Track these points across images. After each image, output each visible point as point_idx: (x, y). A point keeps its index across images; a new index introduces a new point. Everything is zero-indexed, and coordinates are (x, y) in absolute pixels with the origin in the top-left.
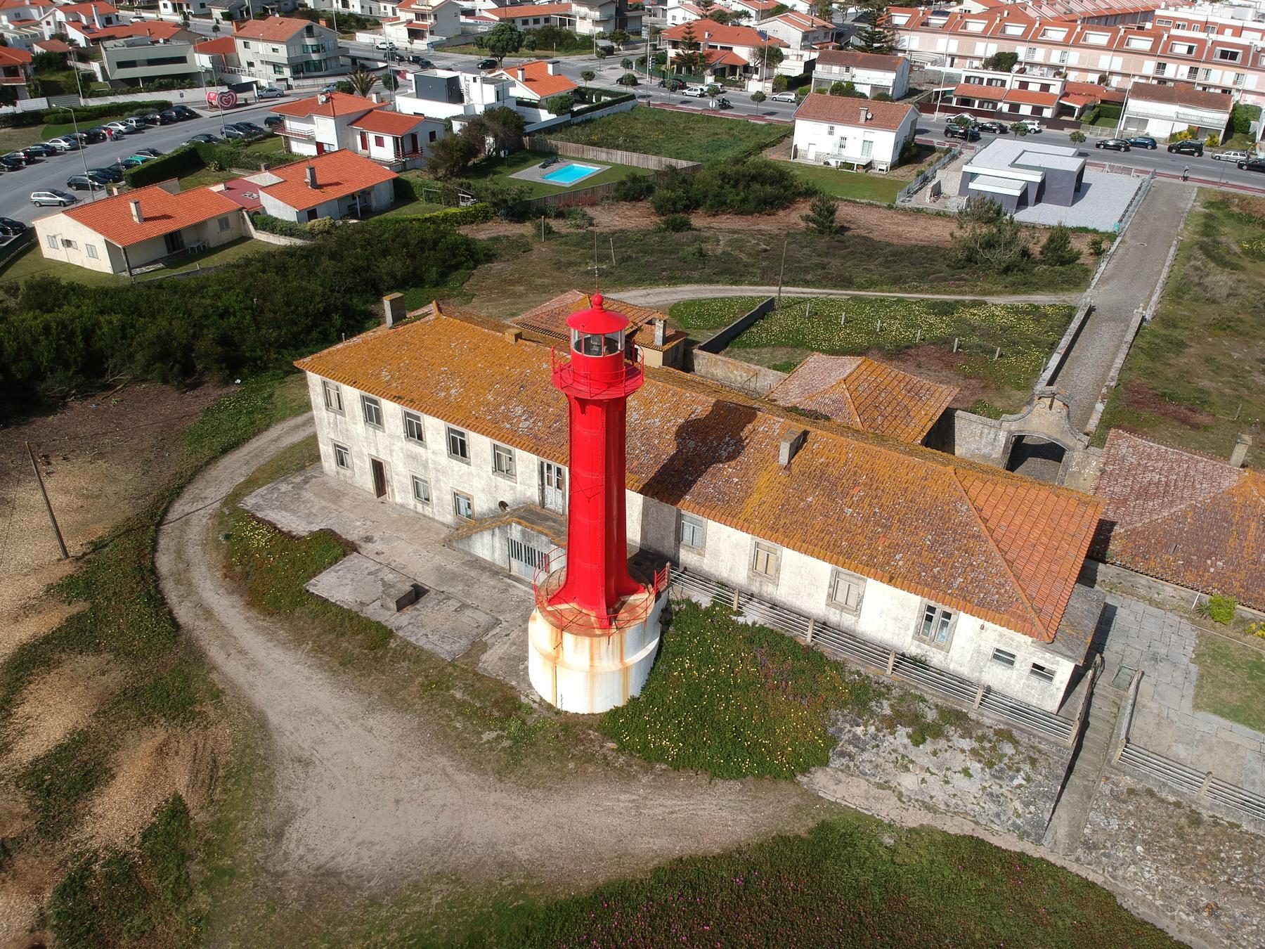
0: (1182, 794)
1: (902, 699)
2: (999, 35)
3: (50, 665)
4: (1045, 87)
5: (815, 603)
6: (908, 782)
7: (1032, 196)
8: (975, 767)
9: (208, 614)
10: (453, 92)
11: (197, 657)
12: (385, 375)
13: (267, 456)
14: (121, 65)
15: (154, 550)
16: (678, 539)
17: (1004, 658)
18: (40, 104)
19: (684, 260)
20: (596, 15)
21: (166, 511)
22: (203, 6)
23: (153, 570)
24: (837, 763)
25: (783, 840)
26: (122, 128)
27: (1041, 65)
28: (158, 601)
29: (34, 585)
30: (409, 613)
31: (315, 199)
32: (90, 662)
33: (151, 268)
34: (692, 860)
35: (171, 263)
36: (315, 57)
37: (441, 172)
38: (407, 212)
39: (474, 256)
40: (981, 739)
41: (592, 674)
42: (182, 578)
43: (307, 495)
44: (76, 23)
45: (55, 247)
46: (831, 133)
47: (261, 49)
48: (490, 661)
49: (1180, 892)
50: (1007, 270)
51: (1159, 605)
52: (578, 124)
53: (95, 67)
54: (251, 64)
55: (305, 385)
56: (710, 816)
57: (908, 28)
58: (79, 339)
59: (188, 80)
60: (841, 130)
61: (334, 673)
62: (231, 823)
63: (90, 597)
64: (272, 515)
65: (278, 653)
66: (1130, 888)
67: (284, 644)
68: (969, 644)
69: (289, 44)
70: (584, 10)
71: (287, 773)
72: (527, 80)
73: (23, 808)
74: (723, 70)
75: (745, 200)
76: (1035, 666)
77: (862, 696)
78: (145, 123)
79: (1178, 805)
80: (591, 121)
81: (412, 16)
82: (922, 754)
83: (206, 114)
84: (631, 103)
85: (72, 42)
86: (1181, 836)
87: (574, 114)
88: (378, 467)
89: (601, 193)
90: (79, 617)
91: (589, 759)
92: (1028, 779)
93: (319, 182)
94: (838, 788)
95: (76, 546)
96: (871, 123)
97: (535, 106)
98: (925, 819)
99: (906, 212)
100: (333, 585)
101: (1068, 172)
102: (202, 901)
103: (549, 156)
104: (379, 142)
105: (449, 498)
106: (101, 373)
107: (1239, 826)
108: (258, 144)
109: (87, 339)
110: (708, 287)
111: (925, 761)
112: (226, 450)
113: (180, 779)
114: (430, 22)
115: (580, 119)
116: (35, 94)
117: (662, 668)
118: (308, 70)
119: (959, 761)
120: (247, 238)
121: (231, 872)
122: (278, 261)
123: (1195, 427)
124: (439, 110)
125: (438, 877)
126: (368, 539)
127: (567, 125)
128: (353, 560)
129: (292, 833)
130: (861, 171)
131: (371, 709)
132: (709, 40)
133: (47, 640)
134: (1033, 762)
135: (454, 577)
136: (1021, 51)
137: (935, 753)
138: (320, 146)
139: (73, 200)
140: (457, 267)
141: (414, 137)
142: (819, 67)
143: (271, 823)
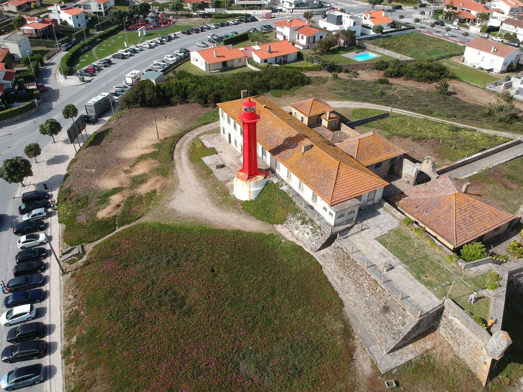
3: (145, 159)
6: (296, 232)
8: (310, 233)
9: (180, 158)
10: (339, 21)
11: (173, 166)
12: (233, 111)
13: (213, 128)
15: (177, 143)
16: (276, 166)
21: (184, 135)
23: (174, 147)
25: (262, 234)
26: (232, 23)
28: (172, 153)
29: (150, 143)
30: (219, 170)
31: (268, 56)
32: (153, 161)
33: (216, 71)
35: (222, 71)
37: (318, 51)
38: (299, 64)
39: (304, 81)
42: (179, 151)
43: (215, 139)
46: (479, 54)
48: (228, 184)
50: (501, 121)
52: (383, 37)
55: (218, 111)
56: (252, 225)
58: (183, 89)
60: (483, 54)
61: (197, 177)
62: (163, 197)
63: (159, 148)
65: (189, 170)
67: (191, 169)
68: (321, 206)
71: (178, 192)
72: (371, 18)
73: (129, 183)
75: (420, 76)
77: (296, 210)
82: (301, 227)
84: (411, 30)
87: (383, 33)
88: (230, 135)
89: (367, 66)
90: (155, 152)
91: (236, 208)
92: (319, 238)
93: (271, 51)
94: (280, 229)
95: (161, 137)
96: (496, 53)
97: (370, 28)
98: (294, 240)
102: (151, 207)
103: (362, 48)
104: (302, 38)
106: (187, 99)
108: (266, 34)
109: (185, 89)
110: (375, 105)
111: (301, 229)
112: (204, 124)
115: (385, 35)
117: (261, 195)
118: (301, 6)
119: (307, 230)
120: (245, 66)
121: (158, 204)
122: (253, 74)
123: (506, 187)
124: (332, 27)
126: (221, 152)
129: (172, 202)
130: (486, 72)
131: (200, 186)
132: (462, 7)
133: (147, 155)
134: (322, 235)
138: (285, 37)
139: (207, 46)
140: (296, 85)
141: (314, 37)
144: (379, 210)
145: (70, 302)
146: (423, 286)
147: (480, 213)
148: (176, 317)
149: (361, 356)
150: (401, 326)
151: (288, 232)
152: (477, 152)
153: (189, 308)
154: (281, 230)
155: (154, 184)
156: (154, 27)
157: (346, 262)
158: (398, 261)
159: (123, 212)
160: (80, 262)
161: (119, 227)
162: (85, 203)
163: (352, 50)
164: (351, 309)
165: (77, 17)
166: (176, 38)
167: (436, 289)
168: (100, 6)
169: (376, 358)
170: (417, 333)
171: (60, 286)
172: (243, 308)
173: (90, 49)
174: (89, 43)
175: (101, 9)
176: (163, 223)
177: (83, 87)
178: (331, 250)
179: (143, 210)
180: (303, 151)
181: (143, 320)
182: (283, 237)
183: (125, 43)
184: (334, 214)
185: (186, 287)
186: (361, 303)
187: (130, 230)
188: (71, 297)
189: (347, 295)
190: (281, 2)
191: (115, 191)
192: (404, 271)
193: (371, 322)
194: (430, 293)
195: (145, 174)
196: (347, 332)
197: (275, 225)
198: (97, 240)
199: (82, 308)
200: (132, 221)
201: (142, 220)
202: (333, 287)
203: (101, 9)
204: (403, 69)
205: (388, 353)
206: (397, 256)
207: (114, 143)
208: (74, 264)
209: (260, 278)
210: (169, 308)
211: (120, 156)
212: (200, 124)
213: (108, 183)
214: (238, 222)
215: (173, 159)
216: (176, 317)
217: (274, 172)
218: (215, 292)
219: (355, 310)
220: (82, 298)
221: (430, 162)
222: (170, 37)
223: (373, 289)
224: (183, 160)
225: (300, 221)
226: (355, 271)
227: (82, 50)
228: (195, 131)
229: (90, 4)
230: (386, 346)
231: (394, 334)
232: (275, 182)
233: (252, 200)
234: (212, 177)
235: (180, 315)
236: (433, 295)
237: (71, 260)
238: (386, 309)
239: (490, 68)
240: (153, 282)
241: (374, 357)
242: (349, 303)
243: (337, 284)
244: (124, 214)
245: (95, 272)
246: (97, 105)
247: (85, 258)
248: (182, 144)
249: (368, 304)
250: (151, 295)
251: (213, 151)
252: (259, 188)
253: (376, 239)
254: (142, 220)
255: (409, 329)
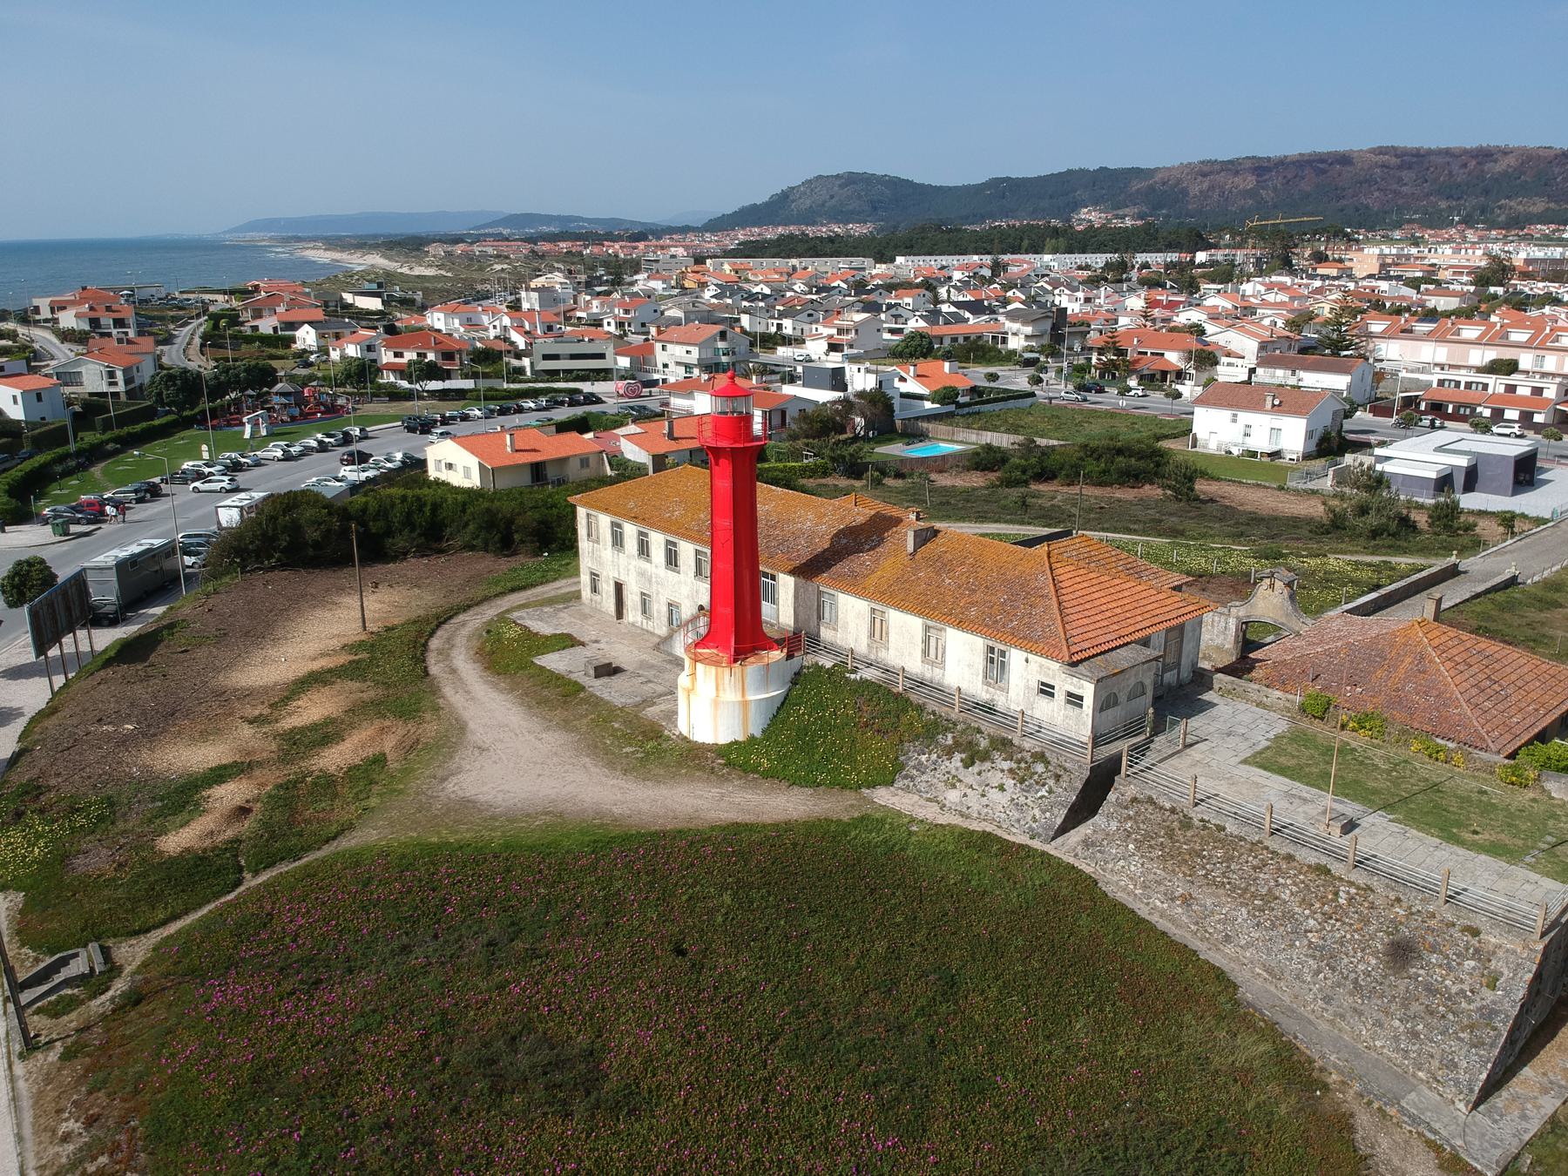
0: (1175, 801)
1: (963, 732)
2: (1497, 341)
4: (1538, 391)
5: (913, 663)
7: (1459, 481)
8: (1009, 783)
10: (837, 379)
11: (435, 691)
14: (546, 357)
16: (820, 618)
17: (1046, 690)
18: (468, 384)
19: (1004, 507)
20: (1029, 330)
21: (450, 618)
22: (643, 325)
23: (425, 645)
24: (899, 783)
25: (828, 821)
26: (532, 405)
27: (1554, 375)
29: (336, 643)
30: (605, 680)
32: (356, 685)
34: (749, 827)
36: (724, 359)
40: (1019, 762)
41: (716, 703)
42: (445, 654)
44: (519, 328)
45: (438, 470)
47: (678, 351)
49: (1159, 883)
51: (1265, 707)
53: (526, 362)
54: (666, 366)
56: (785, 804)
57: (1383, 336)
59: (604, 375)
60: (1245, 417)
62: (413, 770)
64: (528, 623)
65: (494, 695)
66: (1115, 878)
69: (700, 346)
70: (1015, 326)
74: (1152, 377)
76: (1070, 694)
77: (931, 730)
78: (555, 404)
79: (1173, 811)
80: (978, 413)
81: (834, 331)
82: (969, 776)
83: (611, 401)
84: (1029, 401)
85: (512, 343)
86: (1170, 834)
87: (959, 405)
88: (619, 588)
91: (700, 768)
92: (1050, 792)
97: (921, 397)
99: (1297, 492)
100: (553, 661)
101: (1503, 457)
102: (374, 802)
105: (665, 609)
106: (440, 539)
107: (1224, 829)
112: (513, 590)
113: (389, 744)
114: (852, 335)
115: (966, 410)
116: (466, 377)
124: (824, 396)
125: (547, 814)
127: (950, 415)
128: (579, 649)
129: (454, 780)
131: (548, 729)
133: (330, 671)
134: (1058, 777)
135: (652, 667)
136: (1526, 360)
137: (979, 774)
141: (783, 413)
142: (1260, 371)
143: (440, 773)
144: (1207, 697)
145: (70, 1148)
146: (1483, 857)
147: (1508, 670)
148: (577, 1124)
149: (1384, 1143)
150: (1488, 994)
151: (922, 802)
152: (1364, 593)
153: (628, 1086)
154: (895, 799)
155: (372, 739)
156: (293, 419)
157: (1183, 837)
158: (1361, 808)
159: (266, 825)
160: (100, 1004)
161: (256, 873)
162: (101, 819)
163: (890, 441)
164: (1267, 991)
165: (39, 397)
166: (367, 438)
167: (1528, 859)
168: (111, 374)
169: (1444, 1133)
170: (1527, 1032)
171: (15, 1099)
172: (854, 1057)
173: (83, 467)
174: (78, 453)
175: (115, 384)
176: (434, 839)
177: (66, 547)
178: (1109, 816)
179: (343, 812)
180: (910, 548)
181: (433, 1157)
182: (912, 820)
183: (204, 447)
184: (1088, 691)
185: (591, 1015)
186: (1296, 958)
187: (309, 873)
188: (72, 1125)
189: (1229, 949)
190: (660, 366)
191: (219, 775)
192: (1395, 827)
193: (1360, 1014)
194: (1520, 872)
195: (329, 721)
196: (1294, 1068)
197: (865, 791)
198: (164, 923)
199: (131, 1157)
200: (307, 849)
201: (347, 843)
202: (1164, 933)
203: (115, 384)
204: (1051, 462)
205: (1476, 1106)
206: (1346, 796)
207: (201, 654)
208: (73, 1015)
209: (881, 947)
210: (540, 1094)
211: (228, 683)
212: (499, 589)
213: (189, 756)
214: (723, 805)
215: (426, 673)
216: (577, 1124)
217: (814, 641)
218: (717, 1017)
219: (1283, 993)
220: (123, 1121)
221: (1279, 584)
222: (346, 434)
223: (1323, 900)
224: (463, 675)
225: (958, 756)
226: (1229, 859)
227: (59, 469)
228: (485, 607)
229: (82, 369)
230: (1457, 1083)
231: (1472, 1027)
232: (829, 665)
233: (752, 739)
234: (585, 701)
235: (593, 1116)
236: (1534, 876)
237: (58, 1002)
238: (1401, 953)
239: (1275, 448)
240: (445, 1021)
241: (1435, 1132)
242: (1248, 975)
243: (1172, 920)
244: (270, 832)
245: (173, 1020)
246: (126, 568)
247: (119, 986)
248: (448, 640)
249: (1327, 956)
250: (446, 1063)
251: (567, 641)
252: (776, 692)
253: (1245, 762)
254: (347, 843)
255: (1520, 993)
